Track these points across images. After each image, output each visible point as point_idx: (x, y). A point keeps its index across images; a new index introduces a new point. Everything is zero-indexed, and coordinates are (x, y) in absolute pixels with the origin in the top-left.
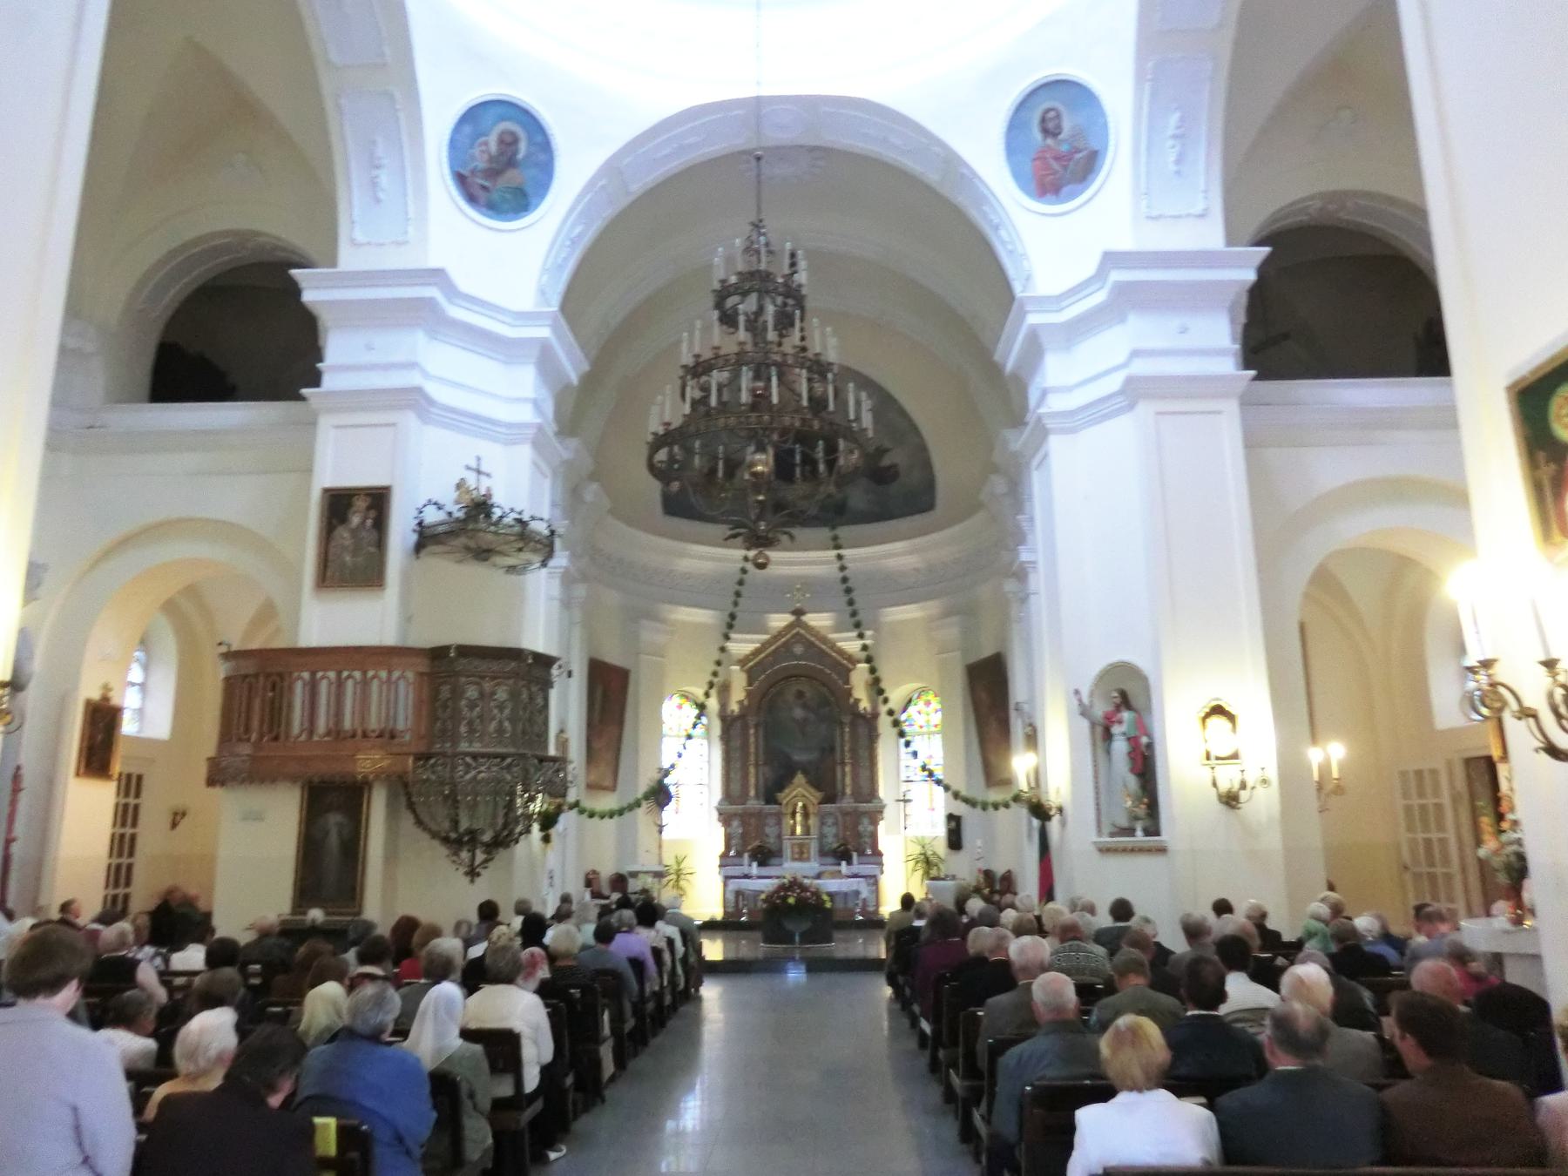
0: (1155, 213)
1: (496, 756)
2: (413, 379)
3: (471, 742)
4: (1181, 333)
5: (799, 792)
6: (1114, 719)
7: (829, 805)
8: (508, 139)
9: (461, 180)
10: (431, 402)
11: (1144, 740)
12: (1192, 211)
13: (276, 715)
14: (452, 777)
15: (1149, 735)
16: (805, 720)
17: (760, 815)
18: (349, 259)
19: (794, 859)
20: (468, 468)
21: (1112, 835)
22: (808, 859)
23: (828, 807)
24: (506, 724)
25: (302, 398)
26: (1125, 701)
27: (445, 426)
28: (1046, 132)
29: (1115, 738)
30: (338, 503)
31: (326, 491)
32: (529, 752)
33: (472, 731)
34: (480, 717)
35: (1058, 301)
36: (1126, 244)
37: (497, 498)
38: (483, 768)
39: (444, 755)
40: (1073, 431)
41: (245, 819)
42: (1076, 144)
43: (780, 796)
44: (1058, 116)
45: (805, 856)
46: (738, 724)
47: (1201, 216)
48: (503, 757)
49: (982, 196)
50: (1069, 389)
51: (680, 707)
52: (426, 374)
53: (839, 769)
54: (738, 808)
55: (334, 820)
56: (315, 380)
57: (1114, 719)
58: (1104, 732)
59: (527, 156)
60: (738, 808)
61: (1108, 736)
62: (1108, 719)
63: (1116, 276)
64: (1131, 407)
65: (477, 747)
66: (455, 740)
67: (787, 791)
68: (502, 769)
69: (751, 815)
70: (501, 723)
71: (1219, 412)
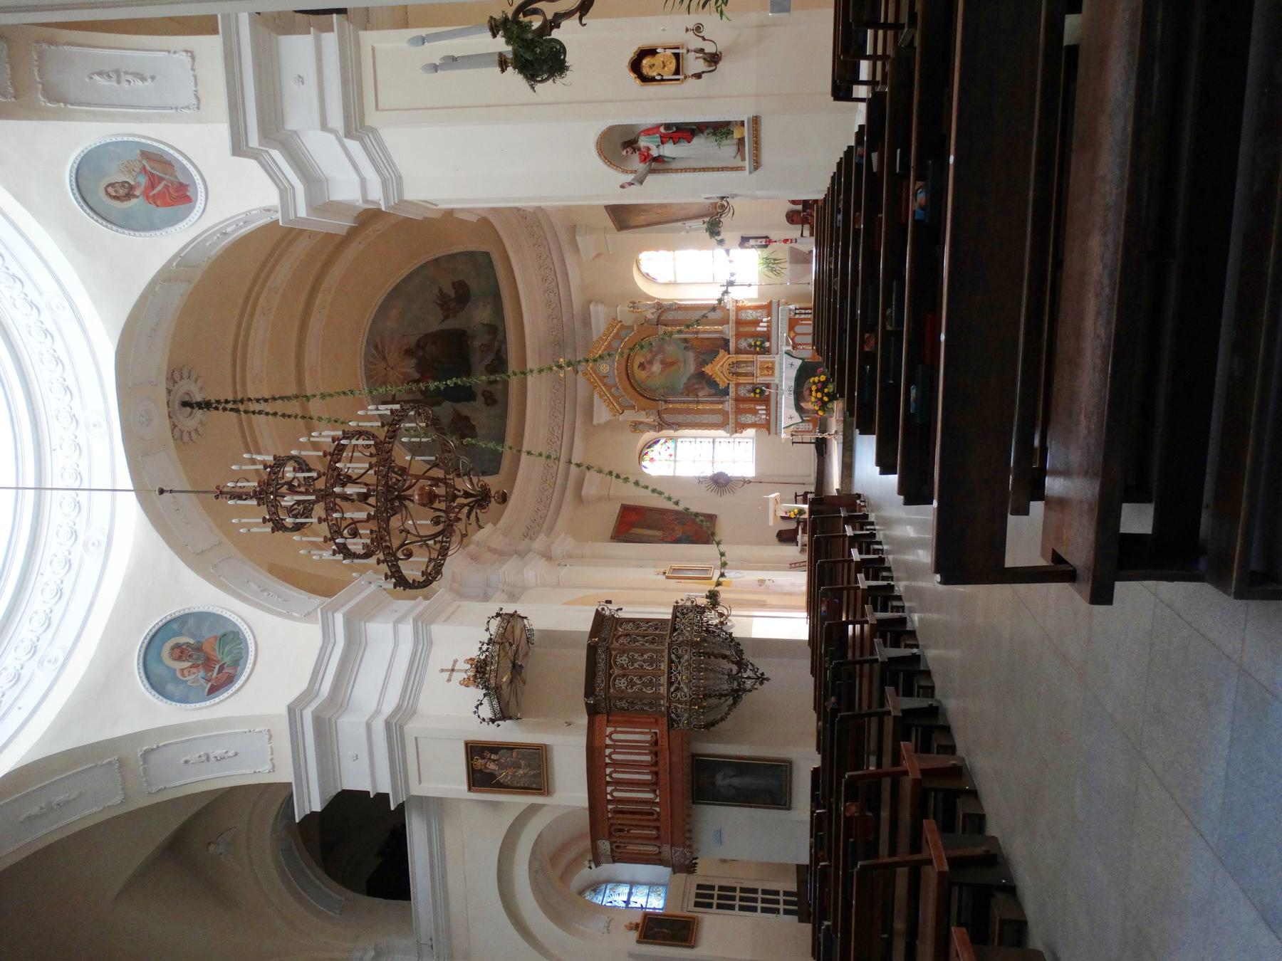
0: (194, 101)
1: (670, 668)
2: (379, 727)
3: (660, 685)
4: (303, 83)
5: (718, 368)
6: (646, 154)
7: (730, 344)
8: (177, 651)
9: (214, 690)
10: (398, 708)
11: (662, 130)
12: (189, 66)
13: (640, 813)
14: (686, 702)
15: (658, 126)
16: (663, 362)
17: (738, 400)
18: (285, 774)
19: (773, 374)
20: (449, 680)
21: (743, 159)
22: (773, 363)
23: (732, 345)
24: (646, 656)
25: (401, 807)
26: (631, 144)
27: (417, 696)
28: (129, 196)
29: (662, 154)
30: (479, 779)
31: (470, 789)
32: (668, 640)
33: (650, 684)
34: (641, 678)
35: (285, 192)
36: (222, 131)
37: (474, 653)
38: (679, 678)
39: (668, 708)
40: (399, 179)
41: (721, 842)
42: (138, 170)
43: (722, 386)
44: (112, 185)
45: (770, 365)
46: (666, 417)
47: (193, 58)
48: (671, 661)
49: (196, 245)
50: (363, 181)
51: (652, 460)
52: (377, 712)
53: (701, 336)
54: (731, 416)
55: (721, 781)
56: (383, 798)
57: (646, 154)
58: (657, 164)
59: (193, 636)
60: (731, 416)
61: (659, 159)
62: (645, 159)
63: (254, 141)
64: (373, 130)
65: (664, 680)
66: (658, 697)
67: (718, 380)
68: (680, 662)
69: (737, 407)
70: (644, 661)
71: (373, 49)
